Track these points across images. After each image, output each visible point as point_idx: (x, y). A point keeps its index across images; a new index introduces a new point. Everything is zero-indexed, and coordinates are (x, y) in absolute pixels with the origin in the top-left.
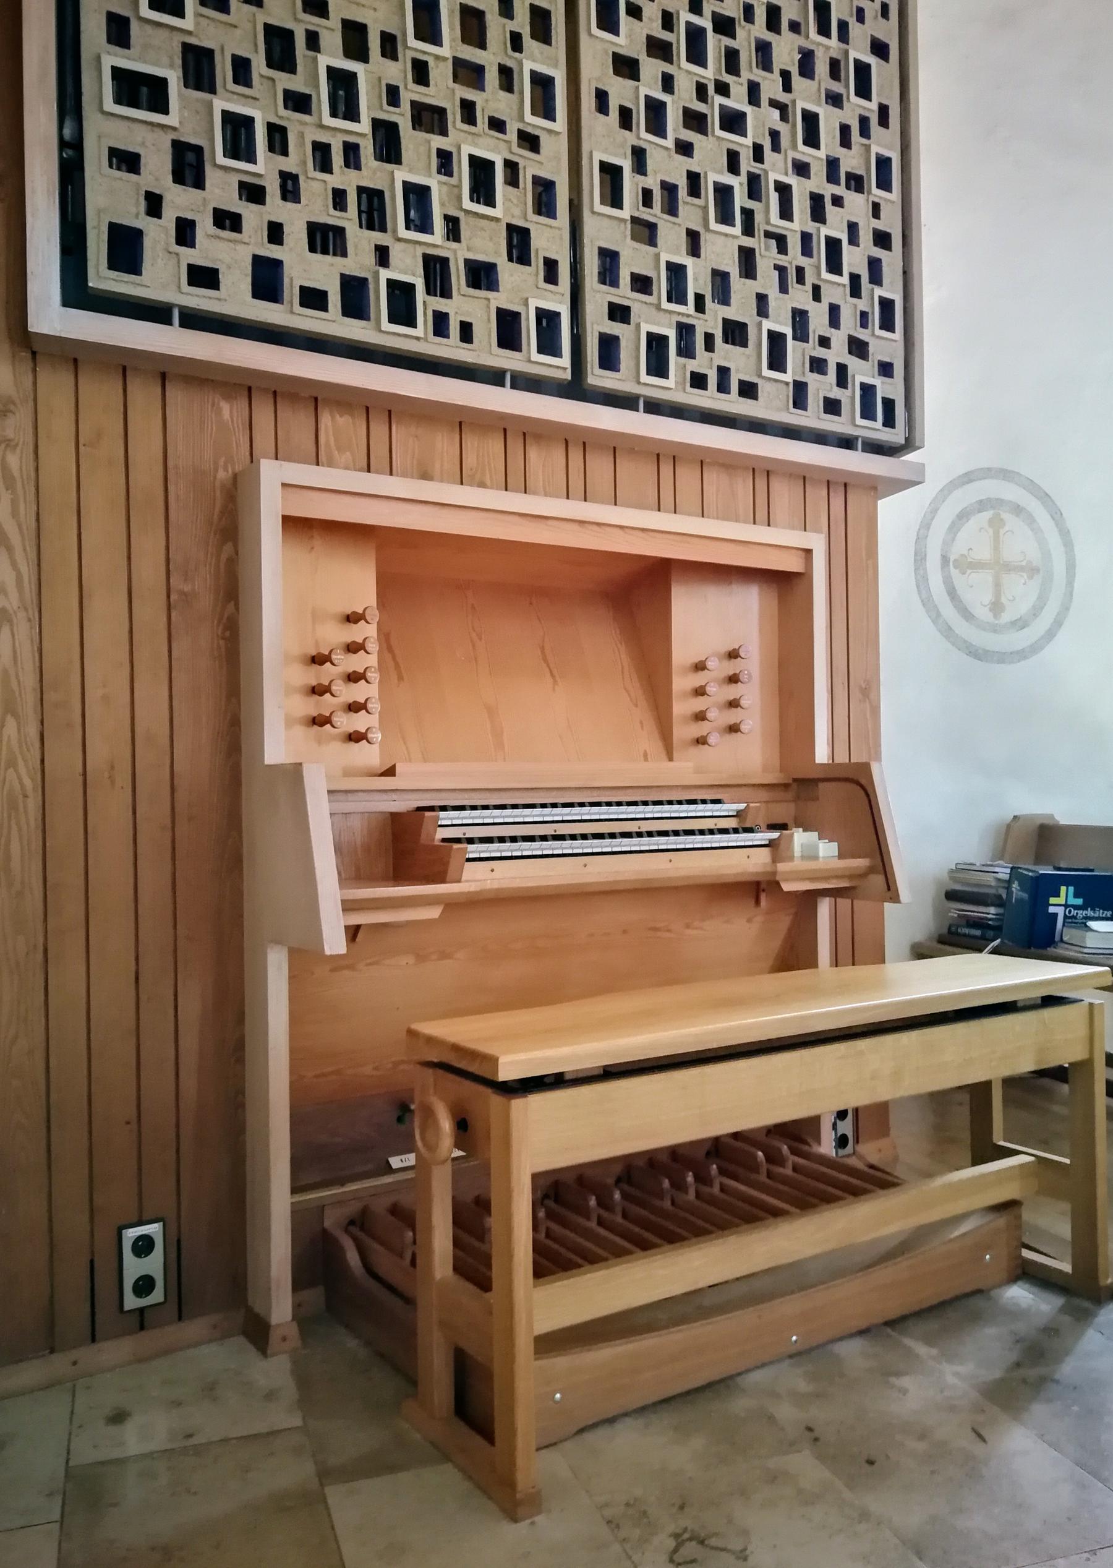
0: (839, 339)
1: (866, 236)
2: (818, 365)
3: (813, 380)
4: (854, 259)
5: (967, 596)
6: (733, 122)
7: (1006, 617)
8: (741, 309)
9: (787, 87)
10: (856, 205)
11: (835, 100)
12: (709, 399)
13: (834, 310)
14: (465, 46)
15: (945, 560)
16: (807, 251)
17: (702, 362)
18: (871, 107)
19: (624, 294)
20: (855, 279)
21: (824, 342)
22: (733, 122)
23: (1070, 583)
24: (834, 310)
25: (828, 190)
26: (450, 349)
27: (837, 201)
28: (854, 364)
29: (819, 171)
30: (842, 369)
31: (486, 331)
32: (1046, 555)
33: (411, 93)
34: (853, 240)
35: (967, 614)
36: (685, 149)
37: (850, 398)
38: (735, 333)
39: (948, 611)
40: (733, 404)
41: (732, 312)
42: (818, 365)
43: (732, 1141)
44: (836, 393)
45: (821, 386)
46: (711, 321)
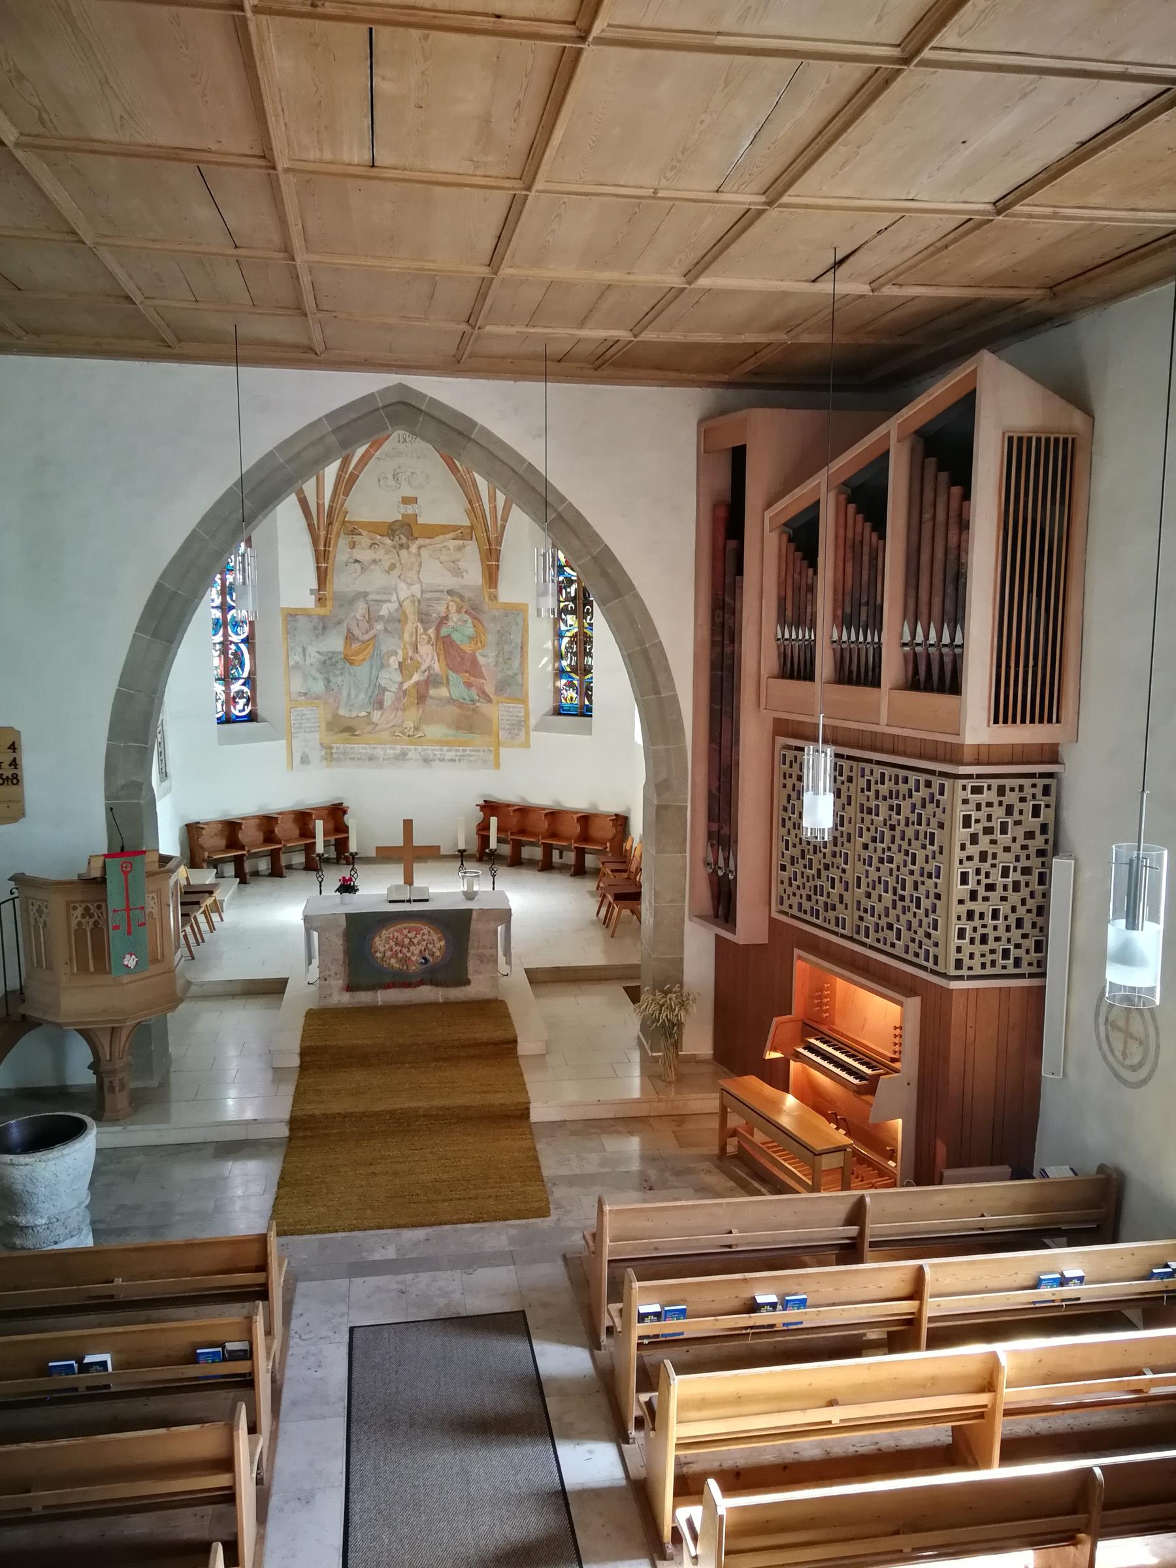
0: (921, 932)
1: (932, 895)
2: (913, 940)
3: (911, 945)
4: (925, 903)
5: (1114, 1043)
6: (891, 860)
7: (1128, 1062)
8: (892, 919)
9: (910, 844)
10: (930, 883)
11: (924, 847)
12: (880, 946)
13: (921, 921)
14: (300, 1021)
15: (1107, 1020)
16: (912, 901)
17: (881, 935)
18: (936, 848)
19: (862, 913)
20: (927, 911)
21: (916, 932)
22: (891, 860)
23: (1157, 1056)
24: (921, 921)
25: (920, 879)
26: (826, 925)
27: (923, 883)
28: (925, 940)
29: (917, 873)
30: (920, 942)
31: (833, 921)
32: (1147, 1036)
33: (823, 861)
34: (927, 897)
35: (1112, 1051)
36: (878, 869)
37: (922, 953)
38: (890, 927)
39: (1105, 1046)
40: (888, 948)
41: (889, 920)
42: (913, 940)
43: (763, 1190)
44: (918, 950)
45: (913, 947)
46: (883, 922)
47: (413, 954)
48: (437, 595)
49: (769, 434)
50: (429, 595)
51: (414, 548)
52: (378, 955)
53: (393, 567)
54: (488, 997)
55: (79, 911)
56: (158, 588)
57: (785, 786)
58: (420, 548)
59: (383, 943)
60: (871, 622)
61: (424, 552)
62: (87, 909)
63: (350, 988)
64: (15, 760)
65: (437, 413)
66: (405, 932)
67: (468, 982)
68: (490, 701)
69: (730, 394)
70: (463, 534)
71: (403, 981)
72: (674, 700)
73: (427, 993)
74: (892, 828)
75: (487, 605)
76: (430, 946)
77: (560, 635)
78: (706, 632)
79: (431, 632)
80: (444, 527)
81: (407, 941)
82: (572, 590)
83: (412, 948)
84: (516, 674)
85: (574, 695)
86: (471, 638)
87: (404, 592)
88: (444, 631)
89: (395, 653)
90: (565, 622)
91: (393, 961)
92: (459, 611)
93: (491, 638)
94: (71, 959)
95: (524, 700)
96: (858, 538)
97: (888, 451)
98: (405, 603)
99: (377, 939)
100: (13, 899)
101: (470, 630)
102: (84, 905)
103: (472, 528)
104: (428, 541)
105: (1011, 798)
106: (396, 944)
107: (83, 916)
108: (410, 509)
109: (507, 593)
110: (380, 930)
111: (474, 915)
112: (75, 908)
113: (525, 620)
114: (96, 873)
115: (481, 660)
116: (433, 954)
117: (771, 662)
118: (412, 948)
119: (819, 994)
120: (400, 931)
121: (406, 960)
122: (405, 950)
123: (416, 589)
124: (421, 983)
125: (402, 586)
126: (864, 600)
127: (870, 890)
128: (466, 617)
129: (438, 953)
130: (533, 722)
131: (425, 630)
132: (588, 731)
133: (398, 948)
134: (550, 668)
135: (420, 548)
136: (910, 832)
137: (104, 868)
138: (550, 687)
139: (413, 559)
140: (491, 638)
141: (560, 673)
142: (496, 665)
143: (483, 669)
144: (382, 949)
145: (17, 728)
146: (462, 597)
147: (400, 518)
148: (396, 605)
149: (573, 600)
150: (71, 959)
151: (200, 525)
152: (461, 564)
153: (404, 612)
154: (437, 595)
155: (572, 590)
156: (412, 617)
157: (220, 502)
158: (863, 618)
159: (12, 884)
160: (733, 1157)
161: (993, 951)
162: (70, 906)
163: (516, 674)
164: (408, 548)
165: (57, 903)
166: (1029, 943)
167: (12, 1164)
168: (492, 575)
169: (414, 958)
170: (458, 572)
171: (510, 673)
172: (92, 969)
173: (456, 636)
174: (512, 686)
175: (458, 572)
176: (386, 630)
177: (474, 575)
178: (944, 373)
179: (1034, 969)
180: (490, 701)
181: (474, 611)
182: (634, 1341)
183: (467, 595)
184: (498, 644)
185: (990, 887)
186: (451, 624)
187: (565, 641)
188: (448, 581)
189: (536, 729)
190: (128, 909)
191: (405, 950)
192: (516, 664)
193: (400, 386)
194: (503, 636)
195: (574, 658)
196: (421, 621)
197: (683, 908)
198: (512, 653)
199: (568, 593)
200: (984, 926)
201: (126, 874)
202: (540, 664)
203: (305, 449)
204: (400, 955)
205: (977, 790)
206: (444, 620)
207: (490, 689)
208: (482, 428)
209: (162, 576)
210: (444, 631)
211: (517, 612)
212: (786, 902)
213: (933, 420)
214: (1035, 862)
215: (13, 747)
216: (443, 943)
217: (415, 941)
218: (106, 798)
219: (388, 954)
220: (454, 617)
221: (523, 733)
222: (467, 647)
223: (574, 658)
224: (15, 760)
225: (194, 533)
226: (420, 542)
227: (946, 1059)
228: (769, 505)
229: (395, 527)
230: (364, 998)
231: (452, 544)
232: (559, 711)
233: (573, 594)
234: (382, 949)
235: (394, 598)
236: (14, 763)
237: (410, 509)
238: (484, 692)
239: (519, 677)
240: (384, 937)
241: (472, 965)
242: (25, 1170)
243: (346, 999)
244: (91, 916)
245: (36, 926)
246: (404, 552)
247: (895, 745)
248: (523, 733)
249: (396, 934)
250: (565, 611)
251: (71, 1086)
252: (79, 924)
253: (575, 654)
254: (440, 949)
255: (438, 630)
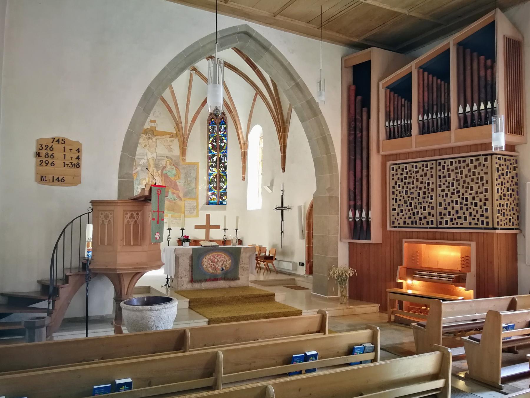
10: (482, 196)
47: (219, 266)
48: (163, 158)
49: (378, 58)
50: (159, 158)
51: (154, 139)
52: (204, 266)
53: (145, 146)
54: (245, 285)
55: (129, 215)
56: (149, 88)
57: (393, 179)
58: (156, 139)
59: (206, 261)
60: (439, 110)
61: (158, 141)
62: (132, 214)
63: (192, 281)
64: (79, 156)
65: (259, 38)
66: (216, 256)
67: (237, 279)
68: (181, 200)
69: (351, 50)
70: (173, 136)
71: (215, 278)
72: (335, 156)
73: (222, 284)
74: (458, 180)
75: (181, 163)
76: (225, 263)
77: (210, 175)
78: (345, 132)
79: (160, 172)
80: (166, 132)
81: (216, 260)
82: (215, 159)
83: (218, 263)
84: (193, 189)
85: (215, 198)
86: (175, 175)
87: (150, 156)
88: (165, 172)
89: (145, 179)
90: (212, 171)
91: (210, 269)
92: (170, 164)
93: (182, 176)
94: (123, 238)
95: (196, 199)
96: (430, 83)
97: (449, 49)
98: (150, 160)
99: (204, 259)
100: (88, 213)
101: (174, 172)
102: (131, 212)
103: (176, 134)
104: (159, 137)
105: (508, 163)
106: (212, 262)
107: (130, 218)
108: (153, 125)
109: (190, 158)
110: (206, 255)
111: (242, 250)
112: (127, 214)
113: (197, 169)
114: (147, 193)
115: (178, 184)
116: (226, 266)
117: (383, 134)
118: (218, 263)
119: (415, 256)
120: (214, 256)
121: (215, 269)
122: (215, 264)
123: (154, 155)
124: (221, 279)
125: (149, 153)
126: (435, 103)
127: (447, 206)
128: (173, 167)
129: (228, 266)
130: (200, 206)
131: (157, 171)
132: (225, 209)
133: (213, 264)
134: (206, 187)
135: (156, 139)
136: (468, 180)
137: (150, 190)
138: (205, 195)
139: (154, 143)
140: (182, 176)
141: (210, 189)
142: (184, 185)
143: (179, 187)
144: (206, 264)
145: (81, 142)
146: (171, 159)
147: (149, 127)
148: (146, 161)
149: (216, 162)
150: (123, 238)
151: (168, 65)
152: (172, 147)
153: (149, 163)
154: (163, 158)
155: (215, 159)
156: (152, 165)
157: (176, 57)
158: (435, 109)
159: (90, 205)
160: (394, 322)
161: (506, 219)
162: (125, 212)
163: (193, 189)
164: (152, 139)
165: (119, 210)
166: (515, 217)
167: (150, 310)
168: (183, 152)
169: (219, 268)
170: (171, 150)
171: (190, 189)
172: (132, 244)
173: (169, 174)
174: (191, 194)
175: (171, 150)
176: (142, 170)
177: (177, 152)
178: (427, 47)
179: (517, 227)
180: (181, 200)
181: (176, 165)
182: (502, 341)
183: (174, 159)
184: (185, 178)
185: (505, 195)
186: (167, 169)
187: (211, 177)
188: (166, 153)
189: (201, 210)
190: (158, 211)
191: (215, 264)
192: (193, 185)
193: (246, 25)
194: (187, 175)
195: (215, 184)
196: (156, 167)
197: (338, 237)
198: (191, 181)
199: (213, 160)
200: (504, 209)
201: (159, 194)
202: (202, 186)
203: (208, 44)
204: (213, 267)
205: (500, 159)
206: (165, 167)
207: (181, 195)
208: (273, 46)
209: (151, 84)
210: (165, 172)
211: (194, 166)
212: (514, 161)
213: (464, 39)
214: (515, 187)
215: (78, 150)
216: (230, 261)
217: (220, 260)
218: (119, 178)
219: (209, 266)
220: (169, 167)
221: (195, 212)
222: (173, 179)
223: (215, 184)
224: (79, 156)
225: (165, 67)
226: (157, 137)
227: (492, 263)
228: (380, 80)
229: (147, 131)
230: (197, 286)
231: (169, 139)
232: (208, 203)
233: (215, 160)
234: (206, 264)
235: (145, 158)
236: (78, 158)
237: (153, 125)
238: (179, 196)
239: (194, 190)
240: (207, 258)
241: (240, 271)
242: (156, 313)
243: (189, 286)
244: (134, 218)
245: (103, 223)
246: (150, 141)
247: (459, 149)
248: (195, 212)
249: (212, 257)
250: (212, 166)
251: (91, 316)
252: (128, 222)
253: (216, 182)
254: (229, 264)
255: (162, 171)
